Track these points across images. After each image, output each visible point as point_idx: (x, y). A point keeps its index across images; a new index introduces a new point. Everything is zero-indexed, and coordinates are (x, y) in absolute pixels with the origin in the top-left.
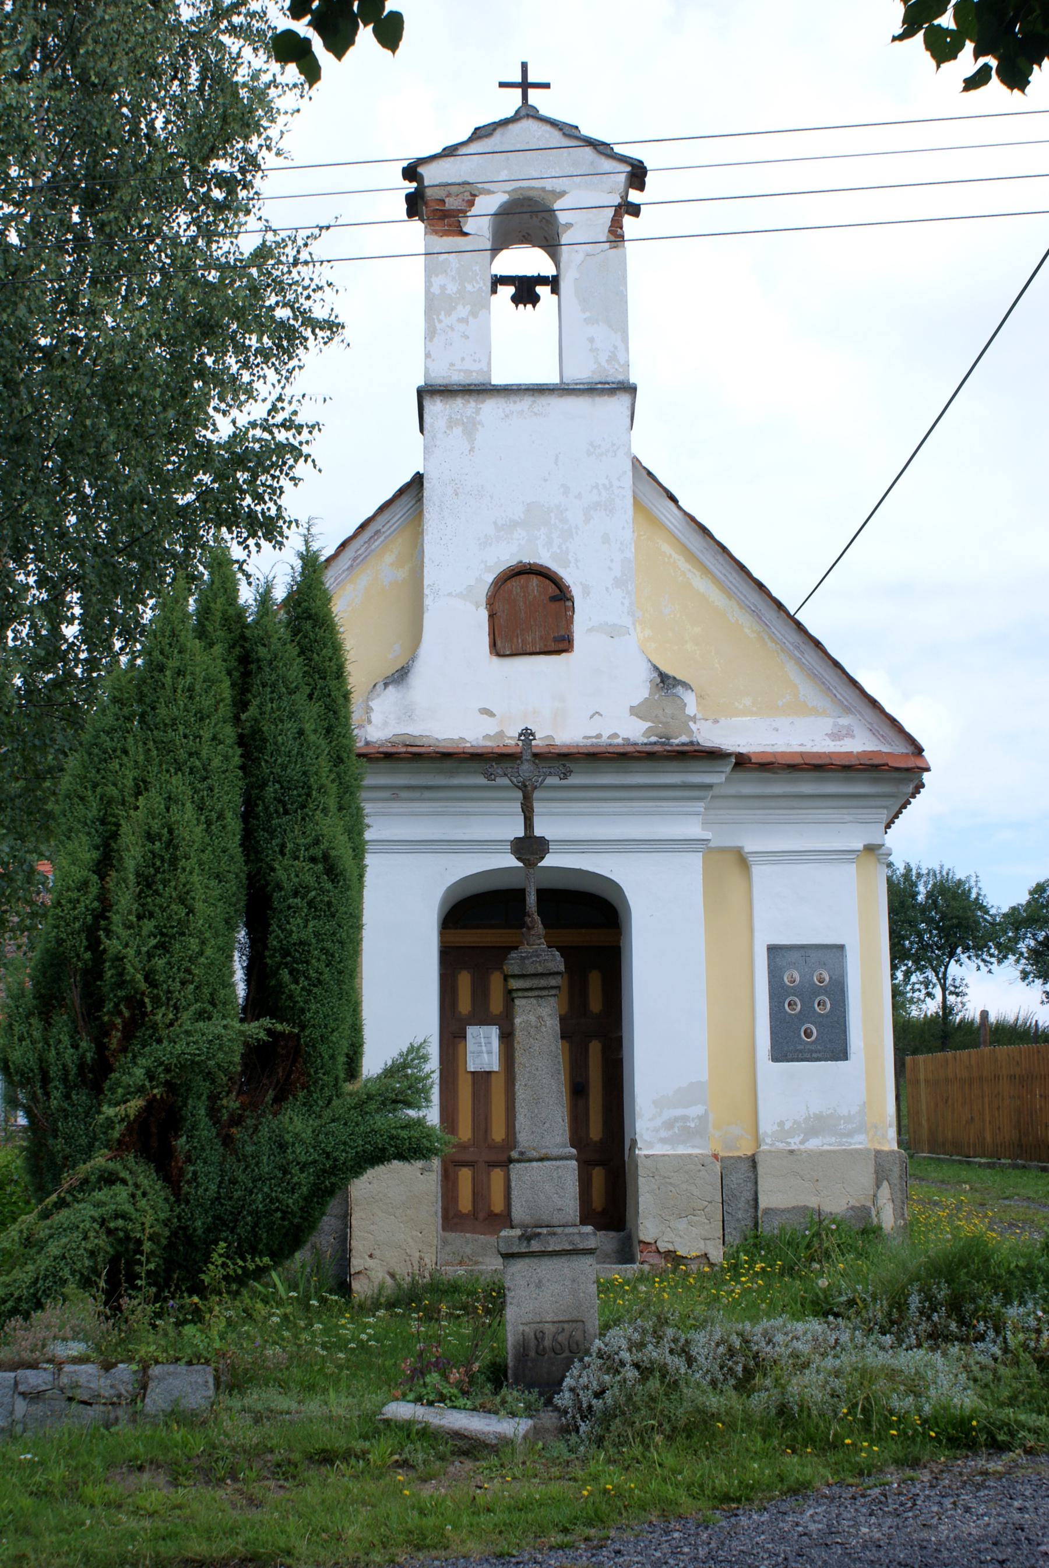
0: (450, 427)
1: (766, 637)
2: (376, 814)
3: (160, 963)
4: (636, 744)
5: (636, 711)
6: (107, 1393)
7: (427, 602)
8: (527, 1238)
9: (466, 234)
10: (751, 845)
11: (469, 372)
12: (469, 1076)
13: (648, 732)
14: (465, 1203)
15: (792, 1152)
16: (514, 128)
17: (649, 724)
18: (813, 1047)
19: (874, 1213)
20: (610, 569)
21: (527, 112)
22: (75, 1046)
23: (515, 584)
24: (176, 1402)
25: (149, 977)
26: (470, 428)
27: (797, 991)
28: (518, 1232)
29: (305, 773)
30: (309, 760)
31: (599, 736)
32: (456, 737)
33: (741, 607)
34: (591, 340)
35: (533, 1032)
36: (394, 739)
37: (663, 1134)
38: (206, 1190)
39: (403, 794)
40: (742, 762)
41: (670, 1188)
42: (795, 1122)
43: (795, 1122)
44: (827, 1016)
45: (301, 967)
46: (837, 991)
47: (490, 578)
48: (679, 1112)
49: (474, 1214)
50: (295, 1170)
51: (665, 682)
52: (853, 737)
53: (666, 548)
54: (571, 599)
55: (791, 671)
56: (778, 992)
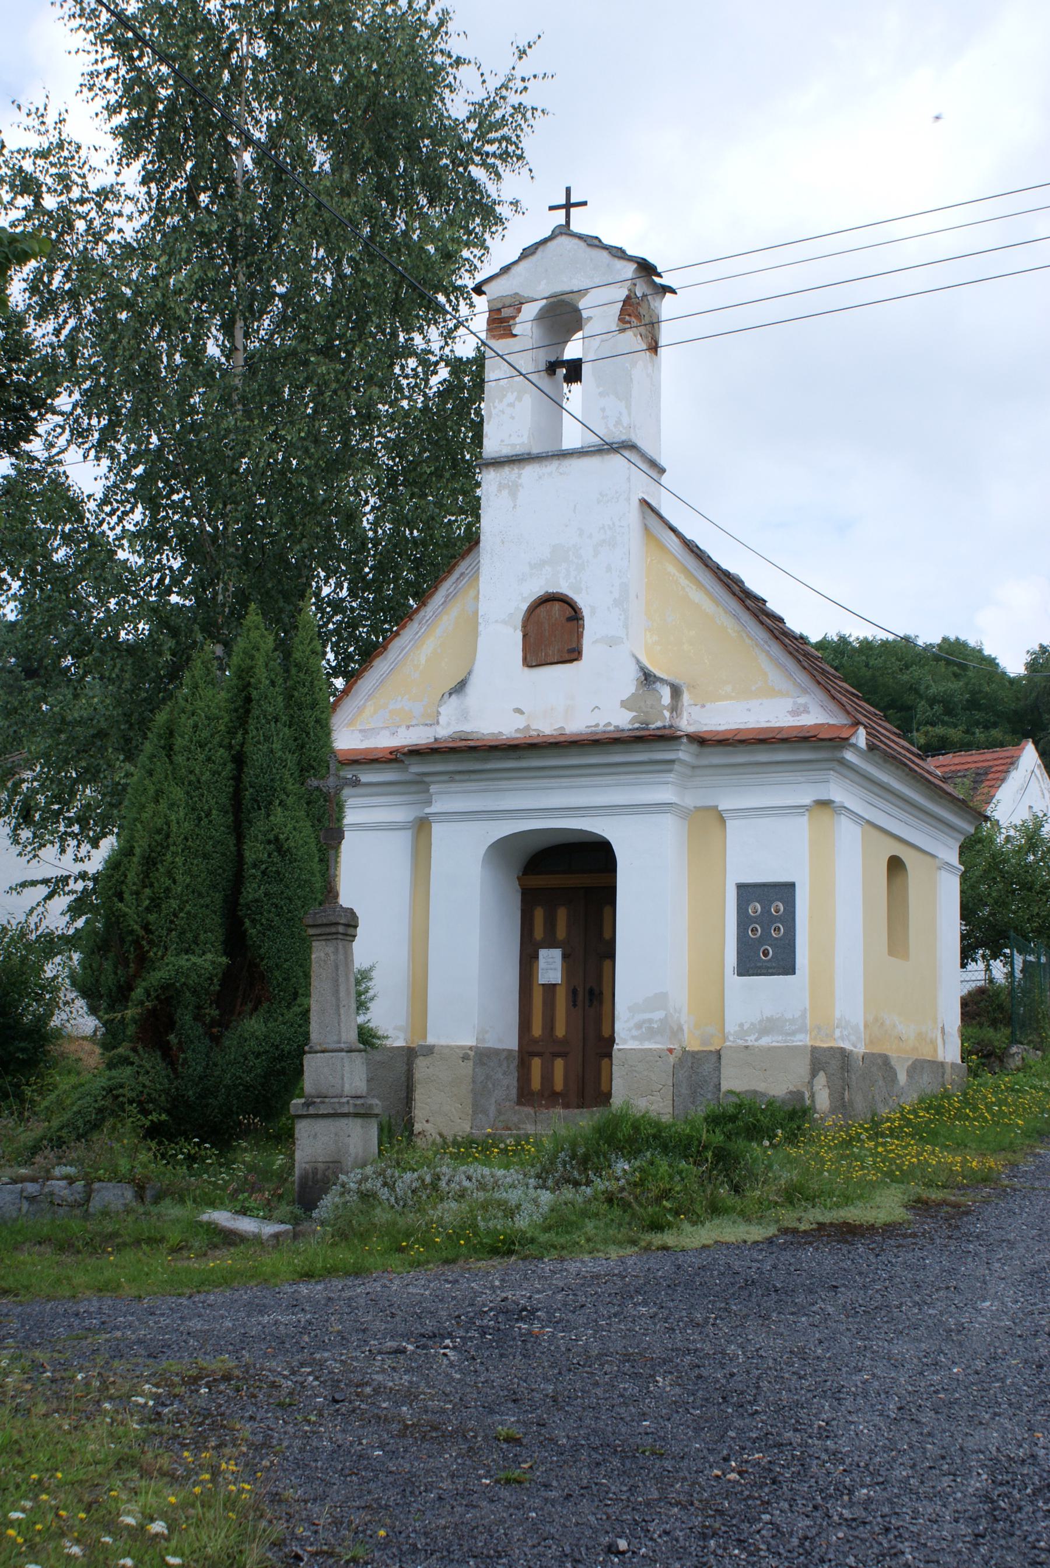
0: (499, 491)
1: (744, 635)
2: (436, 793)
3: (152, 918)
4: (623, 730)
5: (625, 704)
6: (71, 1199)
7: (481, 628)
8: (307, 1105)
9: (515, 336)
10: (726, 803)
11: (513, 445)
12: (541, 988)
13: (634, 720)
14: (536, 1084)
15: (747, 1047)
16: (551, 245)
17: (634, 714)
18: (769, 965)
19: (807, 1095)
20: (611, 592)
21: (564, 230)
22: (116, 974)
23: (542, 610)
24: (105, 1207)
25: (146, 928)
26: (513, 490)
27: (754, 921)
28: (303, 1100)
29: (272, 780)
30: (274, 771)
31: (597, 725)
32: (496, 732)
33: (726, 613)
34: (603, 410)
35: (322, 964)
36: (454, 736)
37: (635, 1033)
38: (195, 1070)
39: (457, 777)
40: (701, 741)
41: (635, 1074)
42: (752, 1024)
43: (752, 1024)
44: (780, 939)
45: (257, 917)
46: (789, 919)
47: (524, 606)
48: (647, 1016)
49: (541, 1094)
50: (251, 1057)
51: (648, 678)
52: (808, 712)
53: (672, 569)
54: (582, 619)
55: (764, 663)
56: (744, 921)
